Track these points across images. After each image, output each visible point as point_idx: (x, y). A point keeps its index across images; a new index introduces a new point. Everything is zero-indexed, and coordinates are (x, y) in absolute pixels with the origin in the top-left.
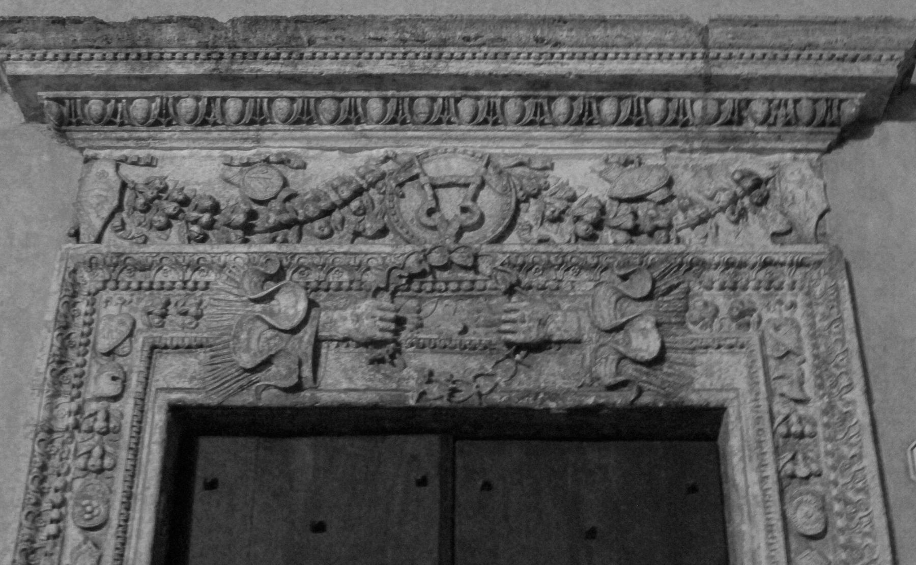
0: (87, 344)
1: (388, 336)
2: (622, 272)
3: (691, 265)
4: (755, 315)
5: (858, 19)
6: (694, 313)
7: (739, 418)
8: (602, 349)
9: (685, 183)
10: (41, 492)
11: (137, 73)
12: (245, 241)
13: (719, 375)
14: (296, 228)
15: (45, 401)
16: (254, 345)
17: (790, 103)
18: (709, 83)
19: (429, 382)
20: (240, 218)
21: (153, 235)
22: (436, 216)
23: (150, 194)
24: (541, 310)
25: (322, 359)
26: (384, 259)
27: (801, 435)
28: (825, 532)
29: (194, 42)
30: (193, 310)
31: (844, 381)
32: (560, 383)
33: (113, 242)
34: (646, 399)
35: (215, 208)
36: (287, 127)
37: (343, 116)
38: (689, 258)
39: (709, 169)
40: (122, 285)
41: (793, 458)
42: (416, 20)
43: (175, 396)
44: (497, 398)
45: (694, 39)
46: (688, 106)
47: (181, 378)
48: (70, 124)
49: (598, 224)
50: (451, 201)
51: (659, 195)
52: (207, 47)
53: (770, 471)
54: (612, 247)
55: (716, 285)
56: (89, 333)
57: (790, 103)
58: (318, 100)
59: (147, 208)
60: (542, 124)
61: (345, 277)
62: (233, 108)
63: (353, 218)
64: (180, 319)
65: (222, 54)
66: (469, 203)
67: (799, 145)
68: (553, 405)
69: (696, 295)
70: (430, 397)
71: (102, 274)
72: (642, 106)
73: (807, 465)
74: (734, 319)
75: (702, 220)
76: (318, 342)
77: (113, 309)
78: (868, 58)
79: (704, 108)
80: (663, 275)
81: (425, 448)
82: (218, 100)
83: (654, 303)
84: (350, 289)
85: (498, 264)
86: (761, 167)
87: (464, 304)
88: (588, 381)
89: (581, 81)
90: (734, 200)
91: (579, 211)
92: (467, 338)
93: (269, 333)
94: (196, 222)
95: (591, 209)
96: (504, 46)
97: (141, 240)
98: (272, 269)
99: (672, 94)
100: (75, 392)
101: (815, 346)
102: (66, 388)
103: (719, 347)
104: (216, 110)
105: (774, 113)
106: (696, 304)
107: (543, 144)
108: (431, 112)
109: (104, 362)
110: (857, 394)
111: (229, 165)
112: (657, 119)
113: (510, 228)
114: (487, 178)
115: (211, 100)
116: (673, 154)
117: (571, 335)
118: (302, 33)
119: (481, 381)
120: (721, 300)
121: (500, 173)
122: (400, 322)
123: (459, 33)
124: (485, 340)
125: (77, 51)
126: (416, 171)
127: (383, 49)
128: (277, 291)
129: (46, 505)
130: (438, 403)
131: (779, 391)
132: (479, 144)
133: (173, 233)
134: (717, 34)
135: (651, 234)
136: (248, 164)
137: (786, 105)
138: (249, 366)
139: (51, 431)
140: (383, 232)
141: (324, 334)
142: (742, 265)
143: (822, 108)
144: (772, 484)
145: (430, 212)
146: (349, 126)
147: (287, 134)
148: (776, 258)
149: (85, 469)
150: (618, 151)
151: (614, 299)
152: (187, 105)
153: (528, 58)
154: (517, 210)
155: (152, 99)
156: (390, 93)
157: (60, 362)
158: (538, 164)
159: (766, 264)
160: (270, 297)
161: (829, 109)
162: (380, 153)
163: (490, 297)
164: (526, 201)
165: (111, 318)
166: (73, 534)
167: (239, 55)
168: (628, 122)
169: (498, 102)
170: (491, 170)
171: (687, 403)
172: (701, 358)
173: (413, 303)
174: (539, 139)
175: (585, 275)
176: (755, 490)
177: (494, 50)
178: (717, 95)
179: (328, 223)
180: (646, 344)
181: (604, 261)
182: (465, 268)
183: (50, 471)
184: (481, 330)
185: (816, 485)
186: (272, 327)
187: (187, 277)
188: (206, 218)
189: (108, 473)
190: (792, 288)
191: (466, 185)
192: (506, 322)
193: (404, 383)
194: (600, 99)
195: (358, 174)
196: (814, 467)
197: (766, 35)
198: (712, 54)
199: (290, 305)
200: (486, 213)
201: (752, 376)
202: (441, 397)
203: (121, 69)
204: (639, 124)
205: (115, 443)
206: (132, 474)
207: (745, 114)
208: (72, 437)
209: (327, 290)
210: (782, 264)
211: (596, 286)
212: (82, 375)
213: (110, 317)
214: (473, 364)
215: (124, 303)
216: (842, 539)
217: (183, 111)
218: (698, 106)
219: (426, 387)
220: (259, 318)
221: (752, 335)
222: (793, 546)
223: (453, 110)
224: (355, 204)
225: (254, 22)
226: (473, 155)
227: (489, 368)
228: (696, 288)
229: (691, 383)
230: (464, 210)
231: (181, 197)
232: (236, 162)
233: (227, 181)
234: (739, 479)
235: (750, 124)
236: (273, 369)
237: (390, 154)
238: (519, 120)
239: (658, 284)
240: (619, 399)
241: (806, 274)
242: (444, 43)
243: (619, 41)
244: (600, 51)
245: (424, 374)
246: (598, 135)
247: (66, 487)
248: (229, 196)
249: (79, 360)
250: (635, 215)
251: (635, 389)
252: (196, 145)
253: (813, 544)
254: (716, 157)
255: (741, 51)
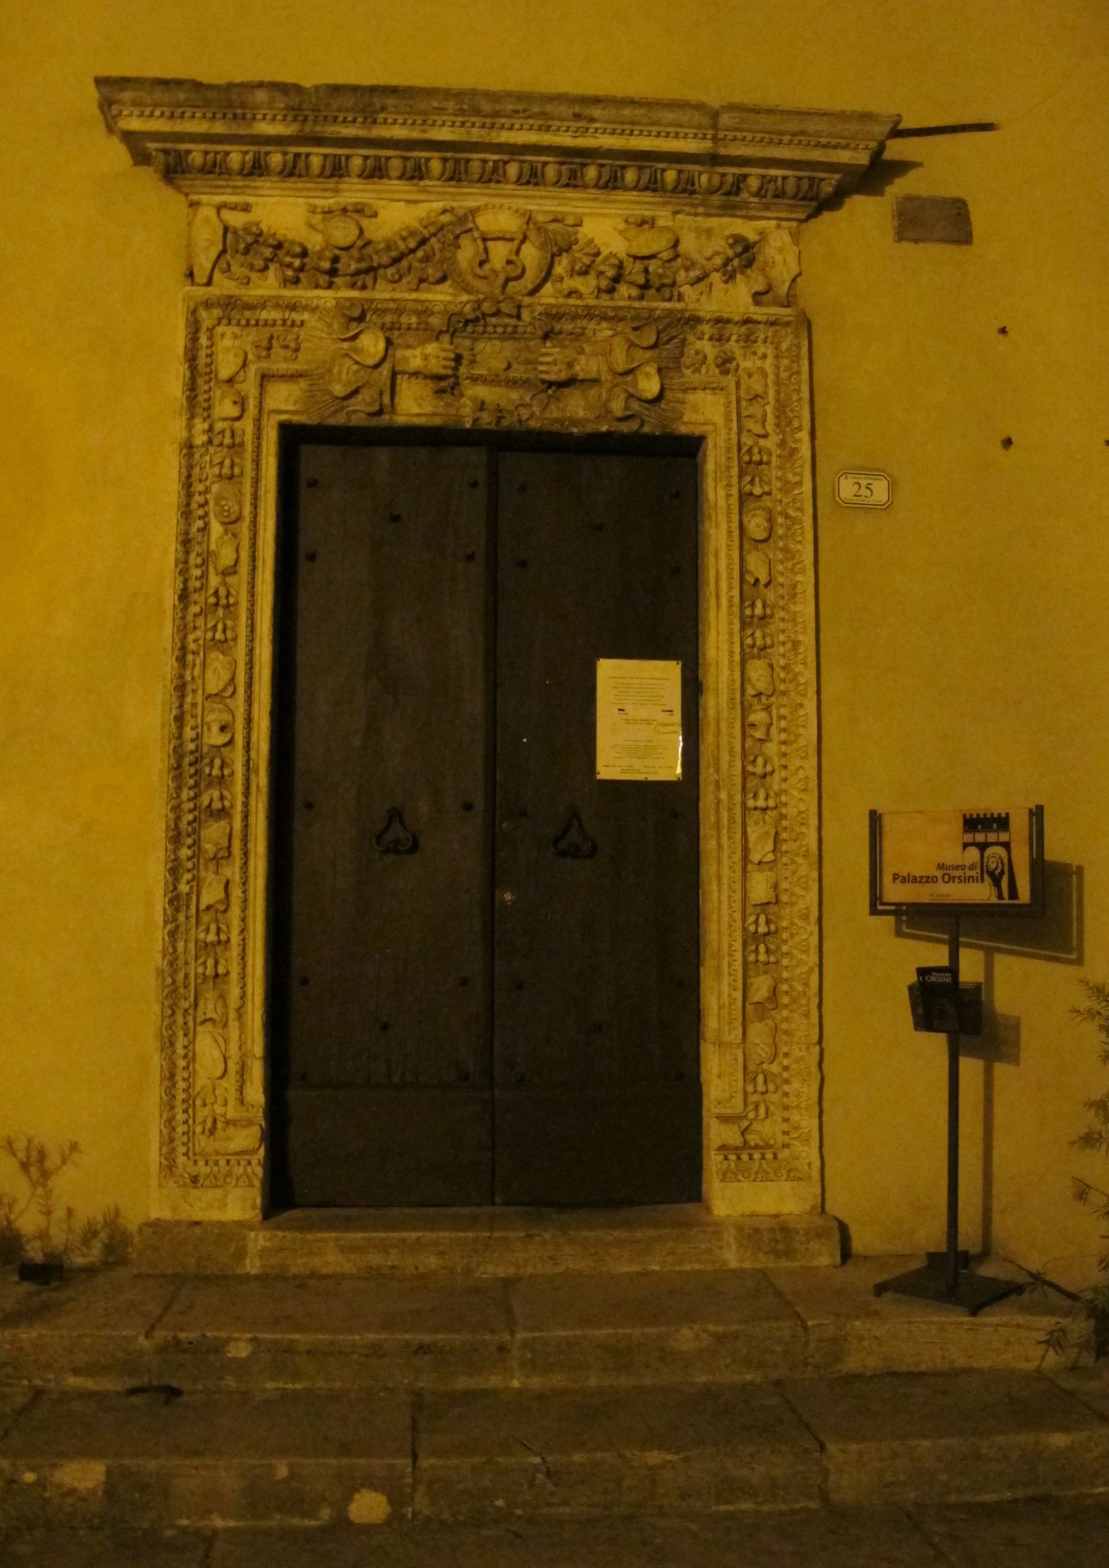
0: (210, 373)
1: (450, 372)
2: (634, 325)
3: (689, 319)
4: (734, 363)
5: (844, 112)
6: (687, 360)
7: (715, 447)
8: (616, 389)
9: (688, 244)
10: (189, 495)
11: (233, 132)
12: (330, 286)
13: (705, 412)
14: (372, 274)
15: (184, 423)
16: (344, 376)
17: (780, 179)
18: (714, 160)
19: (482, 409)
20: (326, 265)
21: (254, 276)
22: (487, 267)
23: (249, 239)
24: (570, 353)
25: (398, 389)
26: (446, 306)
27: (760, 463)
28: (770, 536)
29: (282, 105)
30: (293, 345)
31: (796, 424)
32: (581, 413)
33: (223, 286)
34: (647, 429)
35: (304, 254)
36: (362, 181)
37: (409, 174)
38: (687, 315)
39: (709, 232)
40: (234, 322)
41: (752, 480)
42: (474, 93)
43: (283, 417)
44: (533, 424)
45: (706, 121)
46: (696, 178)
47: (286, 401)
48: (176, 172)
49: (616, 280)
50: (499, 252)
51: (665, 255)
52: (293, 109)
53: (735, 491)
54: (627, 303)
55: (707, 337)
56: (212, 363)
57: (780, 179)
58: (388, 158)
59: (247, 251)
60: (575, 186)
61: (414, 319)
62: (316, 162)
63: (417, 265)
64: (282, 352)
65: (306, 117)
66: (513, 258)
67: (783, 215)
68: (575, 430)
69: (690, 344)
70: (482, 422)
71: (217, 312)
72: (659, 176)
73: (761, 487)
74: (718, 366)
75: (699, 280)
76: (394, 375)
77: (227, 342)
78: (846, 147)
79: (709, 180)
80: (664, 329)
81: (477, 456)
82: (303, 157)
83: (657, 351)
84: (418, 329)
85: (536, 313)
86: (748, 229)
87: (509, 344)
88: (603, 413)
89: (609, 153)
90: (728, 261)
91: (602, 268)
92: (512, 374)
93: (355, 367)
94: (289, 265)
95: (612, 266)
96: (547, 120)
97: (245, 281)
98: (356, 313)
99: (683, 167)
100: (205, 414)
101: (778, 392)
102: (199, 411)
103: (705, 389)
104: (301, 164)
105: (765, 186)
106: (690, 351)
107: (574, 203)
108: (483, 173)
109: (225, 388)
110: (804, 435)
111: (314, 212)
112: (670, 187)
113: (545, 280)
114: (529, 233)
115: (297, 155)
116: (679, 217)
117: (593, 375)
118: (375, 100)
119: (522, 411)
120: (707, 347)
121: (539, 229)
122: (458, 359)
123: (510, 107)
124: (525, 376)
125: (180, 110)
126: (470, 225)
127: (444, 118)
128: (360, 332)
129: (194, 506)
130: (489, 427)
131: (746, 428)
132: (521, 201)
133: (271, 273)
134: (725, 120)
135: (658, 290)
136: (330, 212)
137: (776, 181)
138: (342, 395)
139: (191, 447)
140: (443, 280)
141: (398, 368)
142: (728, 321)
143: (805, 185)
144: (734, 501)
145: (481, 263)
146: (414, 181)
147: (362, 187)
148: (755, 317)
149: (220, 475)
150: (636, 212)
151: (626, 346)
152: (276, 159)
153: (567, 131)
154: (551, 266)
155: (245, 153)
156: (449, 155)
157: (192, 387)
158: (570, 221)
159: (747, 322)
160: (355, 337)
161: (811, 186)
162: (438, 206)
163: (530, 339)
164: (560, 255)
165: (228, 351)
166: (216, 529)
167: (321, 118)
168: (646, 189)
169: (540, 166)
170: (531, 225)
171: (677, 433)
172: (691, 397)
173: (467, 343)
174: (570, 199)
175: (604, 325)
176: (722, 503)
177: (540, 122)
178: (721, 170)
179: (398, 271)
180: (650, 386)
181: (621, 314)
182: (510, 316)
183: (193, 478)
184: (521, 368)
185: (767, 502)
186: (357, 363)
187: (287, 316)
188: (297, 263)
189: (238, 479)
190: (765, 342)
191: (512, 240)
192: (542, 363)
193: (462, 410)
194: (623, 167)
195: (421, 224)
196: (767, 488)
197: (765, 121)
198: (721, 135)
199: (372, 344)
200: (527, 267)
201: (727, 414)
202: (490, 423)
203: (219, 128)
204: (654, 190)
205: (241, 456)
206: (256, 481)
207: (742, 185)
208: (207, 450)
209: (399, 329)
210: (759, 323)
211: (613, 336)
212: (209, 400)
213: (227, 350)
214: (515, 395)
215: (236, 337)
216: (781, 544)
217: (273, 165)
218: (704, 178)
219: (478, 414)
220: (347, 355)
221: (730, 381)
222: (746, 545)
223: (501, 172)
224: (420, 254)
225: (336, 89)
226: (517, 211)
227: (527, 399)
228: (691, 338)
229: (681, 417)
230: (509, 262)
231: (275, 243)
232: (319, 210)
233: (311, 226)
234: (711, 495)
235: (744, 195)
236: (360, 397)
237: (448, 207)
238: (557, 183)
239: (662, 335)
240: (625, 428)
241: (776, 332)
242: (496, 114)
243: (645, 120)
244: (628, 127)
245: (479, 401)
246: (622, 198)
247: (207, 491)
248: (315, 242)
249: (206, 387)
250: (646, 271)
251: (638, 421)
252: (285, 193)
253: (760, 546)
254: (714, 222)
255: (744, 134)
